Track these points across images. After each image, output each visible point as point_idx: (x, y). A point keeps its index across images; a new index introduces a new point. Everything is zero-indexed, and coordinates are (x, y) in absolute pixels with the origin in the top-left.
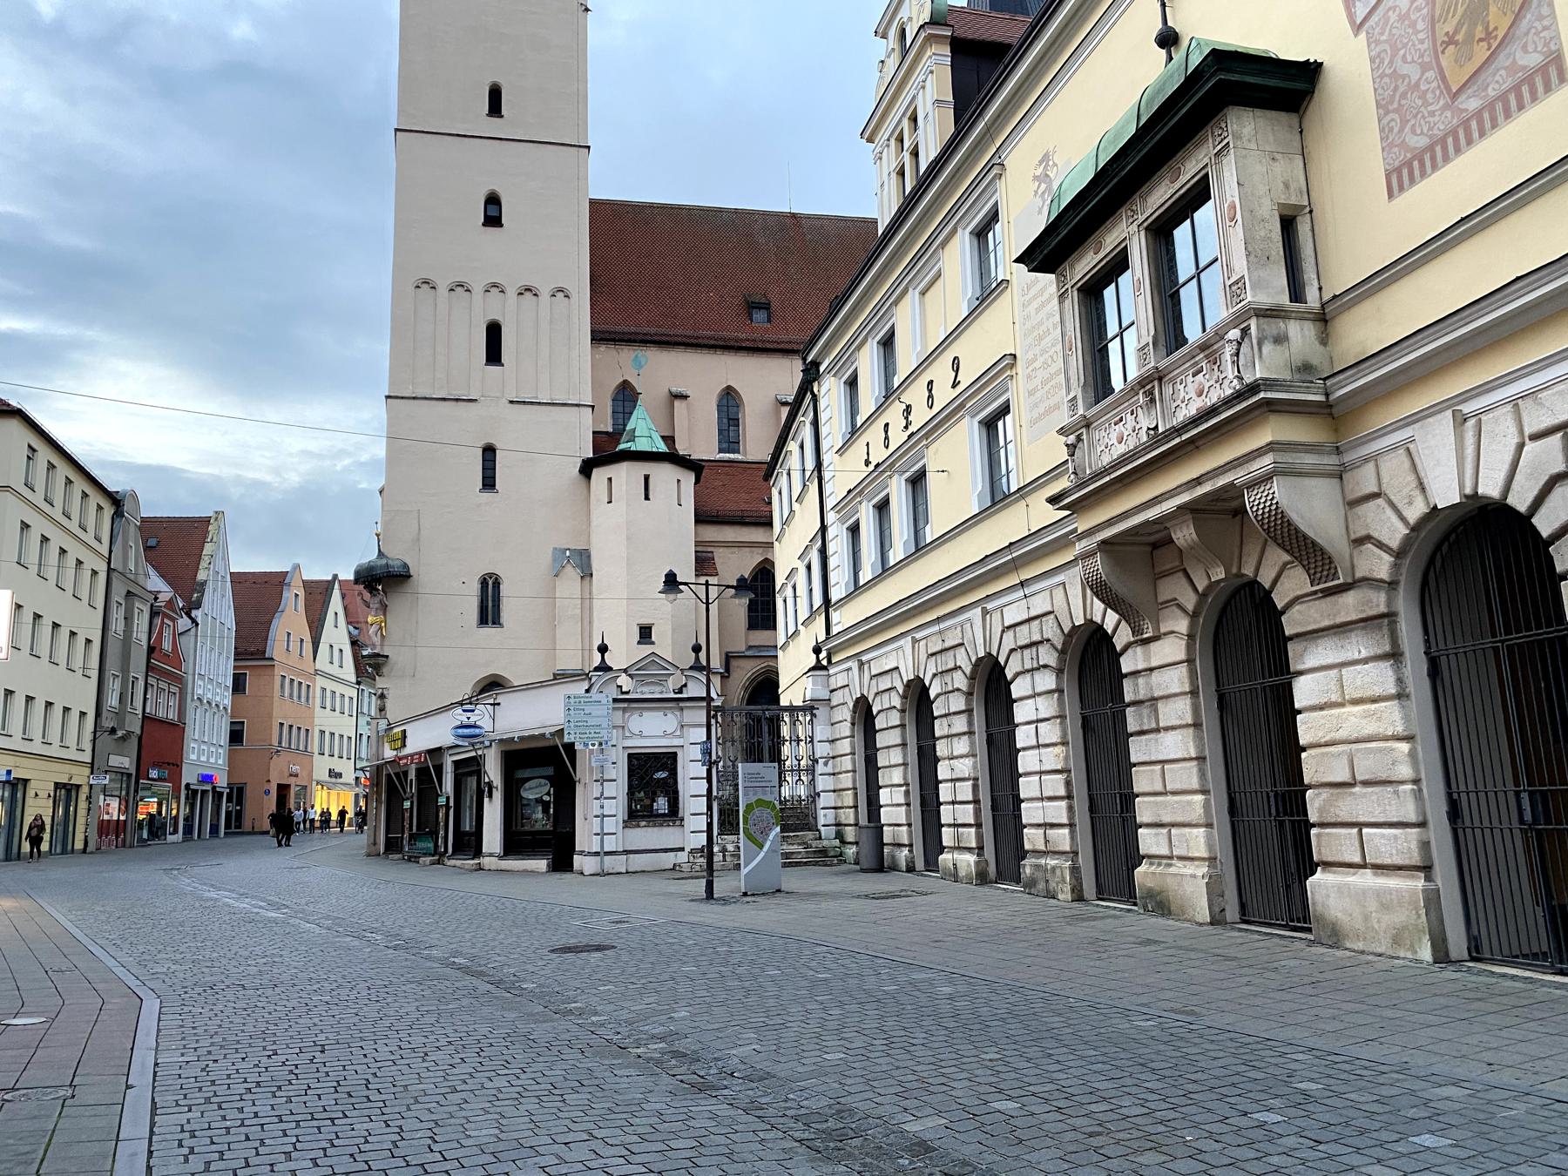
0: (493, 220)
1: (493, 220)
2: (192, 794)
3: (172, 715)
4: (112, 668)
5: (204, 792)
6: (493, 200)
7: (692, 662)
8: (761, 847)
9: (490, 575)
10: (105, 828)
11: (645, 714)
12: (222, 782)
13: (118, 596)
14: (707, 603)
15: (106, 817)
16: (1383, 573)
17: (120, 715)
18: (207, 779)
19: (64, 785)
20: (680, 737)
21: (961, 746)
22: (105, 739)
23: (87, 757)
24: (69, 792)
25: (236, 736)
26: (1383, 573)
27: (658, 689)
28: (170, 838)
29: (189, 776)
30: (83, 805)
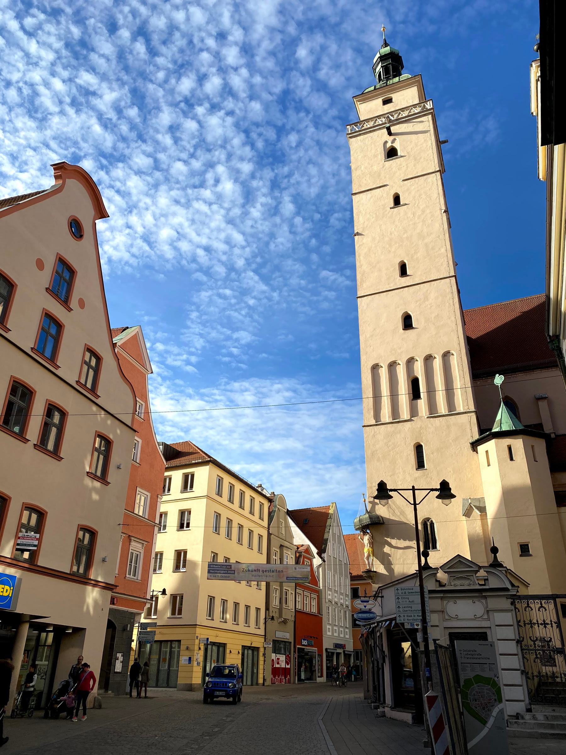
3: (314, 610)
5: (338, 654)
7: (491, 560)
8: (484, 722)
9: (428, 519)
10: (276, 672)
11: (460, 602)
14: (415, 504)
15: (277, 666)
18: (337, 646)
19: (249, 648)
20: (488, 619)
22: (269, 621)
23: (261, 632)
24: (253, 651)
27: (467, 582)
28: (319, 680)
30: (261, 658)
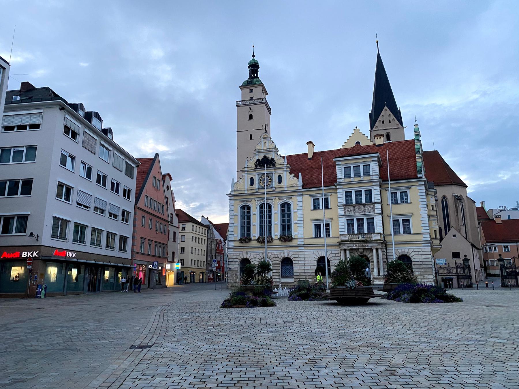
13: (209, 242)
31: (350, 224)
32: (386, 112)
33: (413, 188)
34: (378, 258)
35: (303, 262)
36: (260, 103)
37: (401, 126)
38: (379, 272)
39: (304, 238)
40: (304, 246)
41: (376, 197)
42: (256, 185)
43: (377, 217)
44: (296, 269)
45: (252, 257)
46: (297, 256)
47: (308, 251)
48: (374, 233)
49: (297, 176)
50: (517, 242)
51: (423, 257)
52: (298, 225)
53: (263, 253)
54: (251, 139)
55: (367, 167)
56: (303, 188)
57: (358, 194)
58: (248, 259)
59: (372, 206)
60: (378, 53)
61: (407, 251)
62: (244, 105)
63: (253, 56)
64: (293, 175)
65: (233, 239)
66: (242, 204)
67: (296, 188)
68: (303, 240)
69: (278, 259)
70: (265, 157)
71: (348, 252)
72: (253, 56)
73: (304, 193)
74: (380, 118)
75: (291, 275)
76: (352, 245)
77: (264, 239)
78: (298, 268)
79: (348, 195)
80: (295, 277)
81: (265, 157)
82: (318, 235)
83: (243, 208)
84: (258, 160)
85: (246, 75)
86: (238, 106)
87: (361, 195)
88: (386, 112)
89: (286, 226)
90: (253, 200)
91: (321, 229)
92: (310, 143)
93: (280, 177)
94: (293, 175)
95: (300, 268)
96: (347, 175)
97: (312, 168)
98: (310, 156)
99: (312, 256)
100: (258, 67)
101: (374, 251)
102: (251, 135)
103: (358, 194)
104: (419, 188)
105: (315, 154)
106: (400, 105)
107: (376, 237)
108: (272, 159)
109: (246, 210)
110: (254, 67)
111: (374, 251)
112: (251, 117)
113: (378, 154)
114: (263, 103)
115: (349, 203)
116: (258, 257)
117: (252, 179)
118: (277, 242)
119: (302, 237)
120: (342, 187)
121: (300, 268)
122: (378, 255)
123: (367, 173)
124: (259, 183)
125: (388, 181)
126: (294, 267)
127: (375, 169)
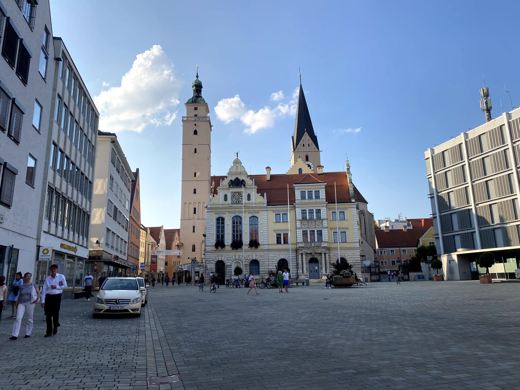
0: (195, 192)
1: (195, 192)
2: (159, 274)
4: (147, 256)
6: (195, 190)
12: (164, 272)
13: (147, 245)
16: (323, 276)
17: (148, 263)
18: (161, 272)
21: (254, 254)
25: (166, 264)
26: (323, 276)
29: (158, 271)
31: (305, 233)
32: (306, 137)
33: (348, 209)
34: (325, 260)
35: (267, 263)
36: (204, 121)
37: (317, 150)
38: (326, 270)
39: (268, 245)
40: (268, 250)
41: (324, 214)
42: (229, 201)
43: (325, 229)
44: (261, 268)
45: (226, 259)
46: (263, 258)
47: (271, 255)
48: (322, 241)
49: (262, 195)
50: (400, 247)
51: (355, 259)
52: (264, 234)
53: (235, 256)
54: (195, 152)
55: (317, 192)
56: (268, 205)
57: (311, 212)
58: (221, 261)
59: (321, 222)
60: (301, 85)
61: (344, 255)
62: (190, 121)
63: (197, 77)
64: (260, 194)
65: (210, 244)
66: (217, 216)
67: (262, 205)
68: (267, 246)
69: (247, 261)
70: (237, 178)
71: (304, 255)
72: (197, 77)
73: (268, 209)
74: (301, 142)
75: (258, 272)
76: (307, 250)
77: (237, 244)
78: (263, 267)
79: (304, 212)
80: (261, 275)
81: (237, 178)
82: (279, 242)
83: (218, 219)
84: (231, 181)
85: (191, 94)
86: (183, 121)
87: (313, 213)
88: (306, 137)
89: (254, 233)
90: (227, 213)
91: (281, 239)
92: (268, 168)
93: (249, 196)
94: (260, 194)
95: (265, 267)
96: (303, 198)
97: (272, 189)
98: (268, 178)
99: (274, 258)
100: (201, 87)
101: (323, 255)
102: (195, 150)
103: (311, 212)
104: (352, 209)
105: (272, 177)
106: (317, 131)
107: (323, 245)
108: (243, 180)
109: (220, 221)
110: (198, 87)
111: (323, 255)
112: (196, 132)
113: (326, 184)
114: (207, 121)
115: (304, 218)
116: (231, 259)
117: (226, 196)
118: (228, 248)
119: (267, 243)
120: (299, 206)
121: (265, 267)
122: (325, 258)
123: (317, 197)
124: (232, 199)
125: (482, 248)
126: (260, 267)
127: (323, 194)
